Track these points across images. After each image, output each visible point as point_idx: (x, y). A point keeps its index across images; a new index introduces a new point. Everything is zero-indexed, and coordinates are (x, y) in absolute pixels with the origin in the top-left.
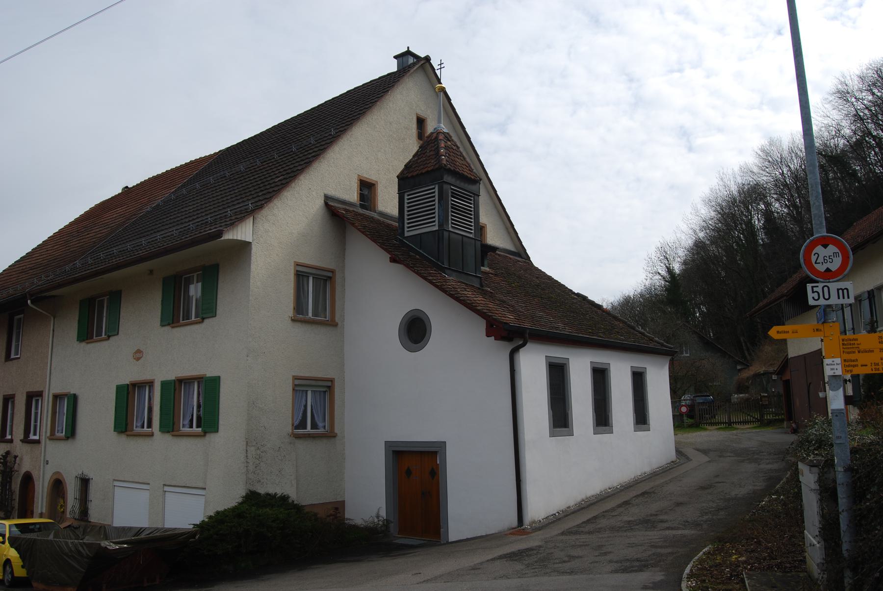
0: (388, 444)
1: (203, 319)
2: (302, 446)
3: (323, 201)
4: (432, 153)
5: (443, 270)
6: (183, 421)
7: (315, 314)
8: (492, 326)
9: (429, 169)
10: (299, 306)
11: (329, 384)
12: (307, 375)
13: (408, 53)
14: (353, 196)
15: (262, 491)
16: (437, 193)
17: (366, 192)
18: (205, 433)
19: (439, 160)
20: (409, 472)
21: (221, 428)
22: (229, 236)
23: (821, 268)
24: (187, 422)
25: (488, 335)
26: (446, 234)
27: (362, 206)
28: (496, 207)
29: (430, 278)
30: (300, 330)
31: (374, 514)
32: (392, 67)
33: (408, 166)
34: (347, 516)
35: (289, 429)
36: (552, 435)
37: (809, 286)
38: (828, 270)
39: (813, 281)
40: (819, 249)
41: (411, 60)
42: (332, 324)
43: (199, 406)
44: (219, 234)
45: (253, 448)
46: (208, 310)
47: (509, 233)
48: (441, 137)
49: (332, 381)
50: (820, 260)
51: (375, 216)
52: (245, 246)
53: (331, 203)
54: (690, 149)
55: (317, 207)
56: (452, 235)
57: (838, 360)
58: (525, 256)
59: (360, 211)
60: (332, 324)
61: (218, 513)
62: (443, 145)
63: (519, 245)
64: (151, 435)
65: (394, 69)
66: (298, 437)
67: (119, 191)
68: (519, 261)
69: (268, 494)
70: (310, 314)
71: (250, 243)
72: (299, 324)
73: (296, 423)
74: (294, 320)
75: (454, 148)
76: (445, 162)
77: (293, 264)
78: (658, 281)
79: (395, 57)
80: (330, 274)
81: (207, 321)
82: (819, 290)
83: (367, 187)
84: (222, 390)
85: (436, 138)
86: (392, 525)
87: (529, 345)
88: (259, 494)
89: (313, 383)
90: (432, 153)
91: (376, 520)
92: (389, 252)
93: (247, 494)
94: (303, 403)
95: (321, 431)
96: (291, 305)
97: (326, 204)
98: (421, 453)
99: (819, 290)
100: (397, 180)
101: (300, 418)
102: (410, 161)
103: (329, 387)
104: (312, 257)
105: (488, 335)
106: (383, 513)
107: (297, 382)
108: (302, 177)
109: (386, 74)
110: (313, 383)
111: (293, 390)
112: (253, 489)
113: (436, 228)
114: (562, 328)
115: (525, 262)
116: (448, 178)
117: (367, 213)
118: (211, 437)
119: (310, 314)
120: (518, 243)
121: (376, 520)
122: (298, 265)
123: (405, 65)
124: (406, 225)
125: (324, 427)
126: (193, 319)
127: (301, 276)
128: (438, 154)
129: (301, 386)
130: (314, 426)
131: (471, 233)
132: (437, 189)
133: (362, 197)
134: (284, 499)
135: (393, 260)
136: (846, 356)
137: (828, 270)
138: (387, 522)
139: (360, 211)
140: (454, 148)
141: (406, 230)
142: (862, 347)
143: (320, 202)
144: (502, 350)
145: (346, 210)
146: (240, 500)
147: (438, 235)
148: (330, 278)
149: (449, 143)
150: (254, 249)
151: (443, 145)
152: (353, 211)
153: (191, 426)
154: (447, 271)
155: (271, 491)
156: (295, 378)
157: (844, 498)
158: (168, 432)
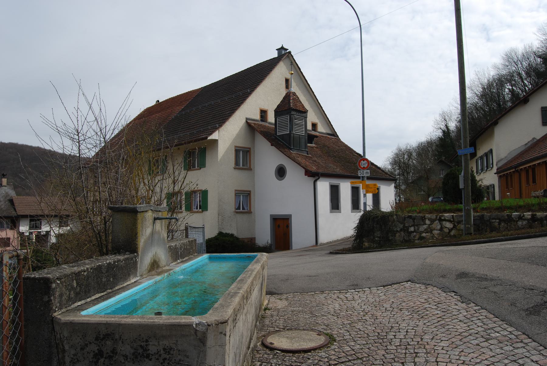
0: (271, 216)
1: (201, 168)
2: (239, 216)
3: (245, 121)
4: (287, 102)
5: (291, 149)
6: (194, 207)
7: (243, 165)
8: (307, 172)
9: (286, 109)
10: (237, 163)
11: (249, 193)
12: (240, 189)
13: (282, 48)
14: (258, 117)
15: (224, 232)
16: (289, 120)
17: (263, 114)
18: (203, 211)
19: (290, 105)
20: (279, 226)
21: (209, 209)
22: (209, 138)
23: (362, 166)
24: (195, 207)
25: (305, 175)
26: (292, 135)
27: (262, 121)
28: (322, 114)
29: (285, 153)
30: (237, 172)
31: (266, 242)
32: (275, 55)
33: (278, 106)
34: (256, 242)
35: (234, 210)
36: (331, 212)
37: (359, 171)
38: (364, 167)
39: (360, 170)
40: (362, 162)
41: (283, 52)
42: (250, 169)
43: (200, 201)
44: (207, 138)
45: (220, 216)
46: (202, 165)
47: (329, 125)
48: (291, 95)
49: (250, 191)
50: (362, 164)
51: (267, 125)
52: (215, 142)
53: (249, 121)
54: (488, 40)
55: (243, 123)
56: (295, 135)
57: (365, 190)
58: (337, 136)
59: (261, 123)
60: (250, 169)
61: (209, 239)
62: (292, 99)
63: (334, 131)
64: (182, 212)
65: (276, 56)
66: (237, 213)
67: (153, 103)
68: (332, 138)
69: (226, 233)
70: (241, 166)
71: (217, 140)
72: (237, 170)
73: (236, 207)
74: (235, 168)
75: (297, 98)
76: (292, 106)
77: (234, 147)
78: (439, 134)
79: (277, 50)
80: (249, 150)
81: (202, 169)
82: (361, 172)
83: (263, 113)
84: (208, 195)
85: (289, 95)
86: (273, 246)
87: (321, 179)
88: (223, 233)
89: (243, 192)
90: (287, 102)
91: (267, 244)
92: (270, 142)
93: (219, 233)
94: (239, 200)
95: (246, 210)
96: (234, 163)
97: (247, 121)
98: (283, 219)
99: (361, 172)
100: (274, 112)
101: (238, 205)
102: (279, 104)
103: (249, 194)
104: (241, 144)
105: (305, 175)
106: (269, 242)
107: (236, 192)
108: (237, 112)
109: (273, 58)
110: (243, 192)
111: (235, 195)
112: (221, 231)
113: (288, 132)
114: (338, 171)
115: (336, 139)
116: (293, 113)
117: (263, 123)
118: (205, 213)
119: (241, 166)
120: (333, 130)
121: (267, 244)
122: (236, 147)
123: (281, 55)
124: (278, 131)
125: (247, 209)
126: (196, 168)
127: (237, 151)
128: (289, 102)
129: (238, 193)
130: (243, 209)
131: (303, 133)
132: (289, 117)
133: (262, 116)
134: (232, 235)
135: (272, 145)
136: (367, 189)
137: (364, 167)
138: (271, 245)
139: (261, 123)
140: (297, 98)
141: (278, 132)
142: (370, 187)
143: (244, 121)
144: (311, 180)
145: (254, 124)
146: (216, 235)
147: (289, 135)
148: (249, 151)
149: (295, 97)
150: (220, 142)
151: (292, 99)
152: (258, 124)
153: (197, 209)
154: (293, 150)
155: (228, 232)
156: (236, 190)
157: (174, 189)
158: (188, 211)
